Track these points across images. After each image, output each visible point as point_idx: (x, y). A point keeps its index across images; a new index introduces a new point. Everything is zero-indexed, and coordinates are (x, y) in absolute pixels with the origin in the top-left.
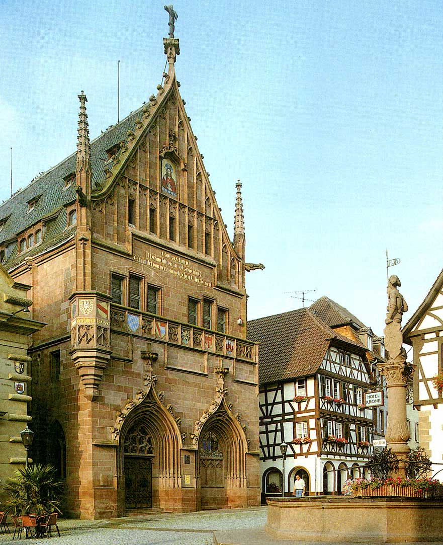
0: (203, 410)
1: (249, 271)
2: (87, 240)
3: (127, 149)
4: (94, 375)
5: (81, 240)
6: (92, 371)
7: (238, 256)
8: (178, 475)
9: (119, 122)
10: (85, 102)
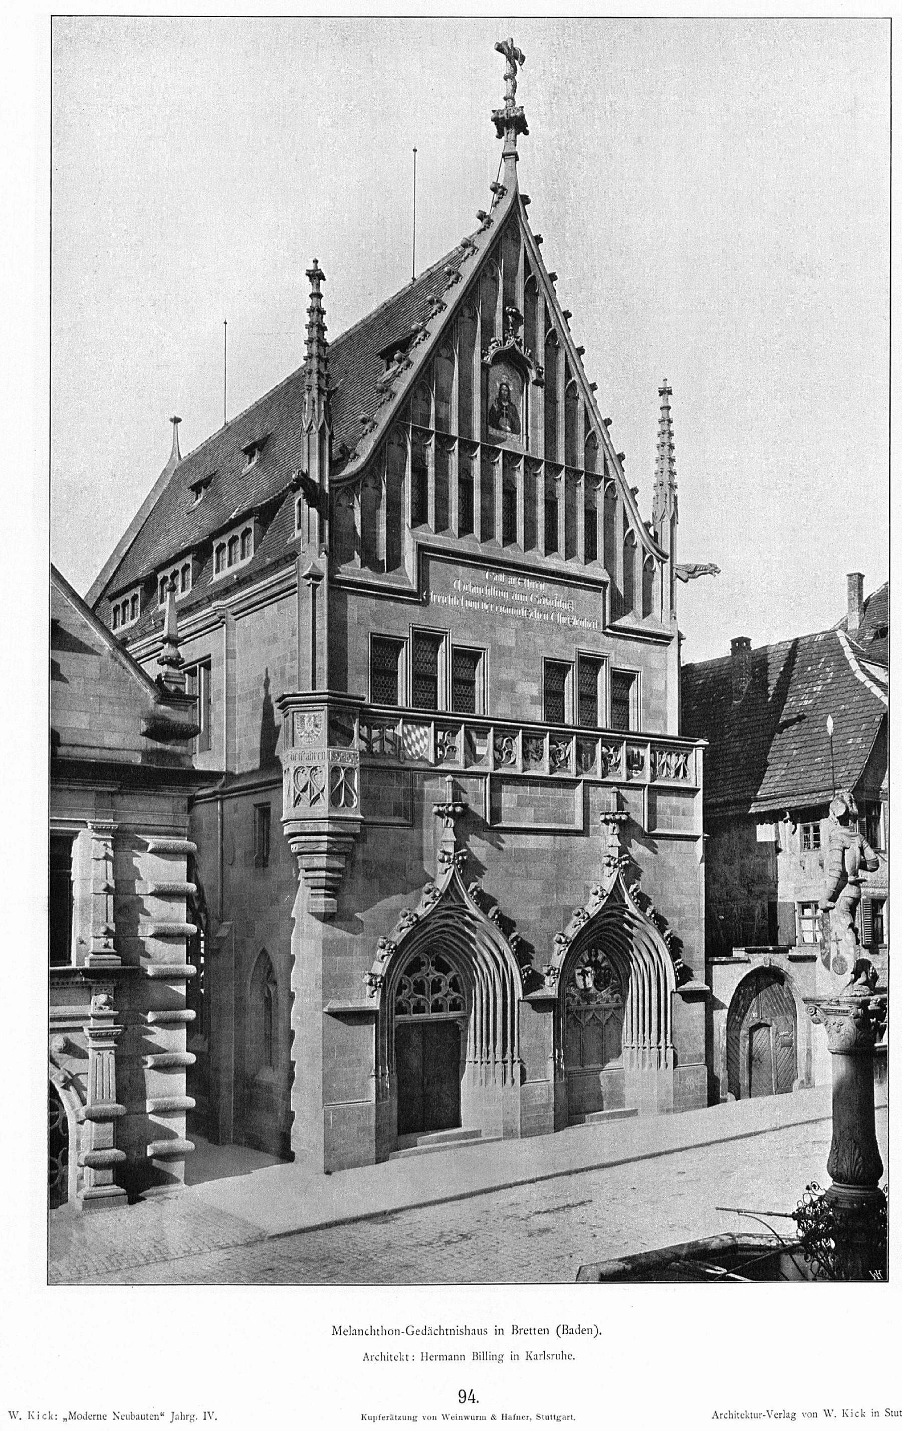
0: (571, 909)
1: (686, 581)
2: (318, 578)
3: (374, 425)
4: (327, 870)
5: (307, 577)
6: (321, 861)
7: (658, 551)
8: (513, 1057)
9: (414, 279)
10: (321, 281)
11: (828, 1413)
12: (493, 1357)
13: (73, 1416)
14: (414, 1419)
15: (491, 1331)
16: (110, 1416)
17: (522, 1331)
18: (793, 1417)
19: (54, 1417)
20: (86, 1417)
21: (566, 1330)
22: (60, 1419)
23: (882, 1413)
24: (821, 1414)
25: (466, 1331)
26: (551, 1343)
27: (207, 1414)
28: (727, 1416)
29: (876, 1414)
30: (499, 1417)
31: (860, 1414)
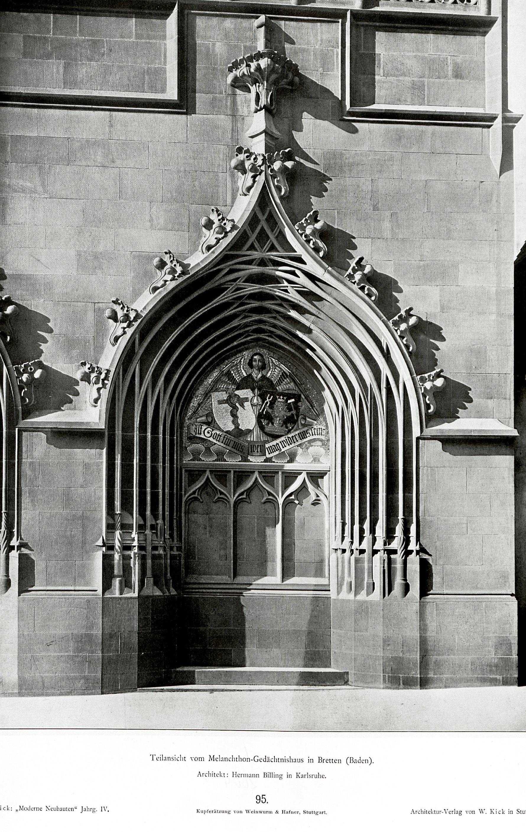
11: (481, 811)
12: (276, 776)
13: (21, 808)
14: (229, 813)
15: (306, 761)
16: (44, 809)
17: (325, 761)
18: (460, 813)
19: (10, 809)
20: (29, 809)
21: (321, 760)
22: (14, 810)
23: (515, 812)
24: (477, 812)
25: (291, 760)
26: (316, 768)
27: (103, 808)
28: (420, 812)
29: (511, 812)
30: (280, 812)
31: (501, 812)
